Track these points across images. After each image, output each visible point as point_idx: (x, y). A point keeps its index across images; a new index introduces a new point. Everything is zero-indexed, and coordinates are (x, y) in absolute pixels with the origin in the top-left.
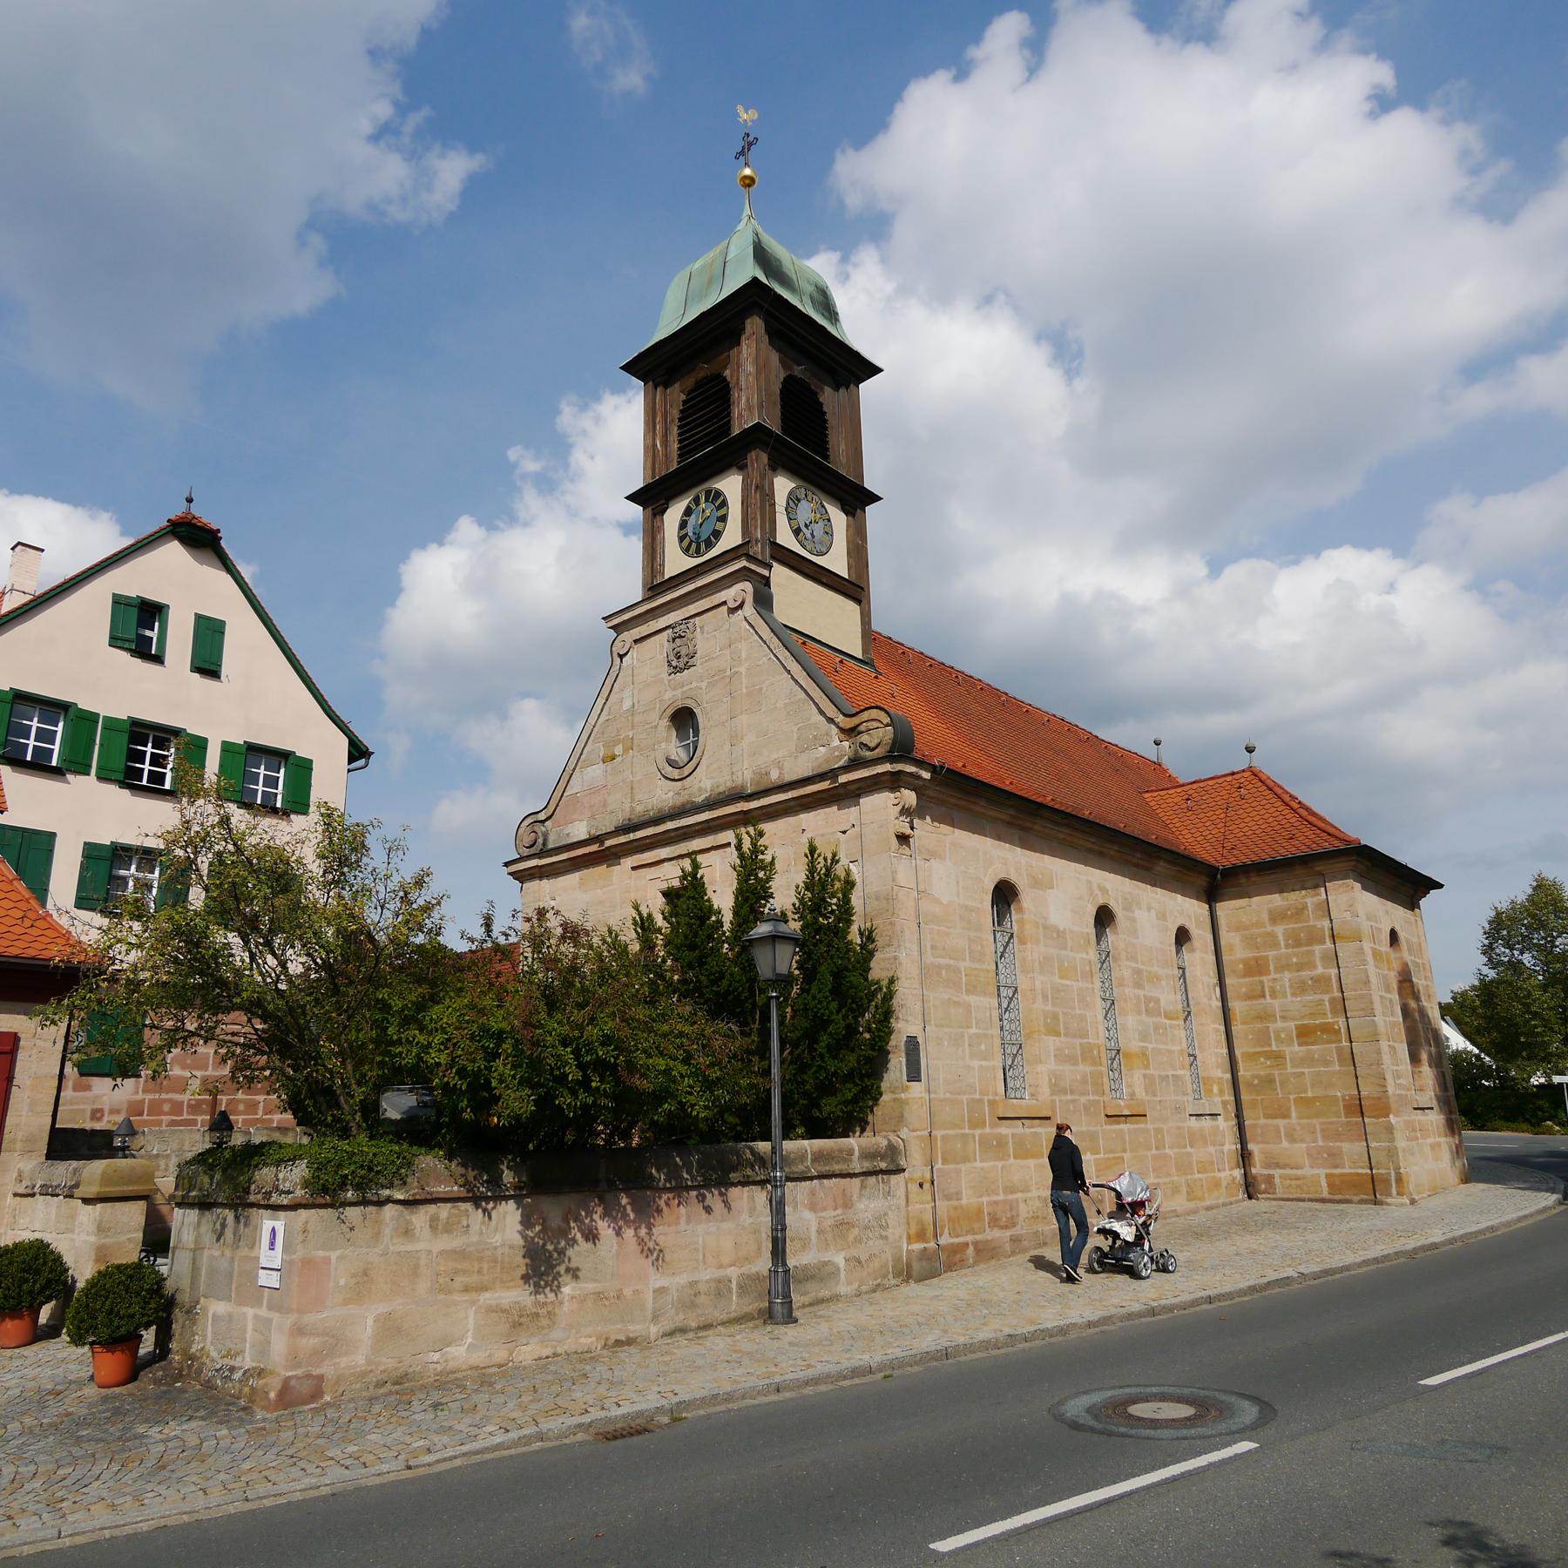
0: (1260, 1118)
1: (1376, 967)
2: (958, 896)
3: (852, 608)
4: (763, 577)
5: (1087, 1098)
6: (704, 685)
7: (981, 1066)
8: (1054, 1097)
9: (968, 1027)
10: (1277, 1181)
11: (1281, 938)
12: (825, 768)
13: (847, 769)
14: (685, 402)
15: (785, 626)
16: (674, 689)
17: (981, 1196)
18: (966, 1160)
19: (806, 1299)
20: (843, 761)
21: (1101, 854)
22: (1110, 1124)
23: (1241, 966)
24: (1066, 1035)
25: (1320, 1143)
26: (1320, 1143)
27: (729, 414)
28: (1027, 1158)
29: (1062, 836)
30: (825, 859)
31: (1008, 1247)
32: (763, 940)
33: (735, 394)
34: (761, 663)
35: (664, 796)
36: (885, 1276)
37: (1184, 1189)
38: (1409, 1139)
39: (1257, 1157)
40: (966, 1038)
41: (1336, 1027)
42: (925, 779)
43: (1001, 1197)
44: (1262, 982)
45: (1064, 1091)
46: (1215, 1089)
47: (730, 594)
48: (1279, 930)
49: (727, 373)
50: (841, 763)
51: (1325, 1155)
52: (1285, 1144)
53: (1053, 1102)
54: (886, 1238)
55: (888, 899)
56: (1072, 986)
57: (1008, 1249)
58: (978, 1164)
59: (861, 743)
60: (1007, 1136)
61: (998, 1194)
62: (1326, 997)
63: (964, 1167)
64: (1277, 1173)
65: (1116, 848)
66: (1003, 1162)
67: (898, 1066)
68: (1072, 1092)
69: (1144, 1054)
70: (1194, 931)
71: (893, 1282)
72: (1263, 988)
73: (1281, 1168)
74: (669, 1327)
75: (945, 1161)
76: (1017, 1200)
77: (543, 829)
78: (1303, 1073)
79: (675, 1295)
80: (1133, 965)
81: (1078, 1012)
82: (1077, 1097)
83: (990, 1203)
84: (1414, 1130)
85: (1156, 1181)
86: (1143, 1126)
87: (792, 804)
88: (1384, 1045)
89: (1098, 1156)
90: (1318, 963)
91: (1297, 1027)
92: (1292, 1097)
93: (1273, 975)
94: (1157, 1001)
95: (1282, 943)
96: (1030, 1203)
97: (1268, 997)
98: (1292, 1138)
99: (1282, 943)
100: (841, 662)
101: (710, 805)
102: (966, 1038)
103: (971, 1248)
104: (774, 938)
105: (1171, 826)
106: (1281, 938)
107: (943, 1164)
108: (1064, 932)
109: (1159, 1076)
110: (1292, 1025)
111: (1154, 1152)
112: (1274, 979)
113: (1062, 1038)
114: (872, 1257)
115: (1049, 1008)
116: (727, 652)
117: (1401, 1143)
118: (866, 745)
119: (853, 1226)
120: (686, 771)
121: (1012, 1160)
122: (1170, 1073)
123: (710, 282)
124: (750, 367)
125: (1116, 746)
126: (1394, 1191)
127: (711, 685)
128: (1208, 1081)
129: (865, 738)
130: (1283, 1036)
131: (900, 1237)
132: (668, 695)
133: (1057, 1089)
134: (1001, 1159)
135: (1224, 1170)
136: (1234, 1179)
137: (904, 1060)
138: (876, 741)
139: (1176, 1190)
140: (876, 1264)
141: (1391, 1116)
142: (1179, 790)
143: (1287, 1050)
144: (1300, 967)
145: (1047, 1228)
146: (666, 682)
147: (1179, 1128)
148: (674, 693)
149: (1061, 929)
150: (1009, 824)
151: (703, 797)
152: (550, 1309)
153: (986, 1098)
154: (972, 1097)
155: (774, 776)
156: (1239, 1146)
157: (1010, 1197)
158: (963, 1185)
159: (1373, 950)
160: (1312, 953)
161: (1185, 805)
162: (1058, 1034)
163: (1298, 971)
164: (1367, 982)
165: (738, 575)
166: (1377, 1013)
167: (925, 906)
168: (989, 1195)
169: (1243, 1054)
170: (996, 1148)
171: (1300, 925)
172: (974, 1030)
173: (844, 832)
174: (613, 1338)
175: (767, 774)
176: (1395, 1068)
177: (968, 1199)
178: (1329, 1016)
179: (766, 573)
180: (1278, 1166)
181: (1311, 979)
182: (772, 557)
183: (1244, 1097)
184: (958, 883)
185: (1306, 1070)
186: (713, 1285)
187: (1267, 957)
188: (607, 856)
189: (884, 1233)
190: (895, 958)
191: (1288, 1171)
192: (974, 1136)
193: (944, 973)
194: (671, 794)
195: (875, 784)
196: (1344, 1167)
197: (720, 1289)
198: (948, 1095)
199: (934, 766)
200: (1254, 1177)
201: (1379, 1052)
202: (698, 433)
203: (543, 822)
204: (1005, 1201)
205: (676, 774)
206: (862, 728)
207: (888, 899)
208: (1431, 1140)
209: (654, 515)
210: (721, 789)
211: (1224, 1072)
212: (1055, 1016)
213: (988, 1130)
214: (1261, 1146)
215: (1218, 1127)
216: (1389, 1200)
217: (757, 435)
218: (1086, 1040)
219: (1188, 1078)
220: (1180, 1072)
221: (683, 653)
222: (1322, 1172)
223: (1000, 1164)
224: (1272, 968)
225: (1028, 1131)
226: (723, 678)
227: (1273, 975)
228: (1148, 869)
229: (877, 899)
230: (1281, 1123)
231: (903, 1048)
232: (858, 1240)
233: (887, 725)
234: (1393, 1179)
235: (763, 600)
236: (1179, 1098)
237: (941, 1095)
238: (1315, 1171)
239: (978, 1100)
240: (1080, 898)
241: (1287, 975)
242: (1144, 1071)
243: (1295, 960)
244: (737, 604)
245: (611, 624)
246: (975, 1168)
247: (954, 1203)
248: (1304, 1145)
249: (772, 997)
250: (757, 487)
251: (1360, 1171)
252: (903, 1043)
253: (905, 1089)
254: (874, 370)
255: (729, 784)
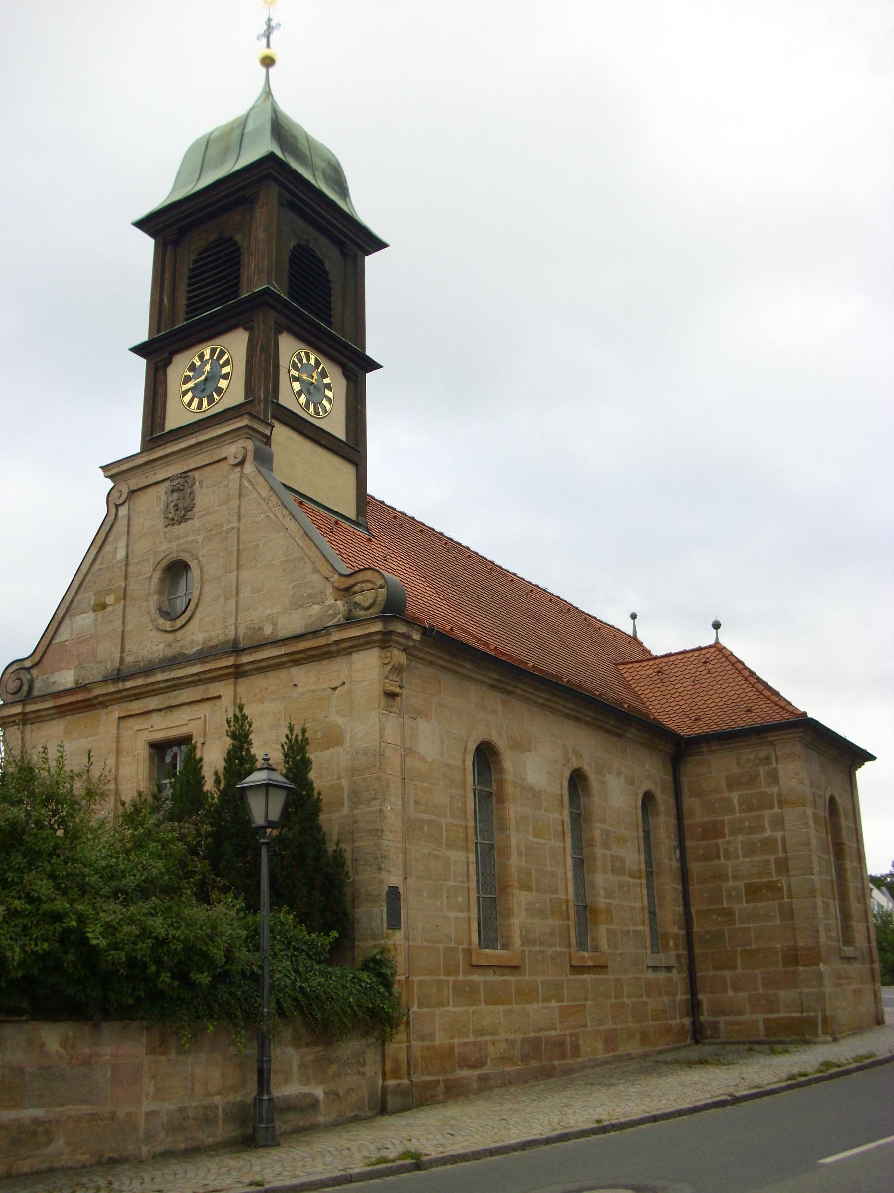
0: (709, 970)
1: (816, 830)
2: (442, 754)
3: (347, 471)
4: (265, 436)
5: (555, 949)
6: (200, 538)
7: (458, 917)
8: (523, 948)
9: (446, 880)
10: (722, 1026)
11: (736, 803)
12: (318, 626)
13: (340, 627)
14: (195, 262)
15: (282, 484)
16: (170, 542)
17: (452, 1038)
18: (441, 1004)
19: (286, 1127)
20: (336, 620)
21: (577, 720)
22: (574, 974)
23: (700, 829)
24: (538, 890)
25: (761, 991)
26: (761, 991)
27: (238, 277)
28: (496, 1004)
29: (541, 701)
30: (286, 743)
31: (475, 1085)
32: (256, 787)
33: (245, 258)
34: (258, 520)
35: (155, 648)
36: (361, 1108)
37: (638, 1036)
38: (836, 985)
39: (705, 1006)
40: (445, 890)
41: (779, 885)
42: (416, 641)
43: (472, 1039)
44: (717, 844)
45: (532, 943)
46: (671, 944)
47: (232, 450)
48: (735, 796)
49: (238, 237)
50: (335, 622)
51: (764, 1002)
52: (730, 993)
53: (523, 952)
54: (363, 1074)
55: (375, 755)
56: (545, 844)
57: (475, 1086)
58: (451, 1008)
59: (355, 603)
60: (479, 983)
61: (469, 1037)
62: (772, 858)
63: (437, 1011)
64: (722, 1019)
65: (591, 714)
66: (475, 1007)
67: (379, 915)
68: (541, 944)
69: (608, 910)
70: (659, 796)
71: (368, 1114)
72: (718, 849)
73: (725, 1015)
74: (159, 1149)
75: (420, 1005)
76: (486, 1042)
77: (29, 676)
78: (749, 928)
79: (165, 1118)
80: (603, 826)
81: (549, 869)
82: (546, 949)
83: (461, 1045)
84: (840, 978)
85: (614, 1027)
86: (603, 976)
87: (285, 659)
88: (819, 901)
89: (563, 1004)
90: (767, 826)
91: (746, 886)
92: (739, 950)
93: (727, 838)
94: (623, 860)
95: (737, 808)
96: (498, 1045)
97: (722, 859)
98: (736, 988)
99: (737, 808)
100: (336, 523)
101: (204, 655)
102: (445, 890)
103: (442, 1085)
104: (268, 786)
105: (642, 697)
106: (736, 803)
107: (418, 1007)
108: (540, 793)
109: (622, 930)
110: (741, 884)
111: (613, 1000)
112: (728, 842)
113: (534, 893)
114: (349, 1090)
115: (524, 864)
116: (225, 507)
117: (828, 989)
118: (359, 605)
119: (333, 1063)
120: (179, 623)
121: (482, 1006)
122: (632, 928)
123: (226, 151)
124: (261, 235)
125: (595, 618)
126: (820, 1031)
127: (207, 539)
128: (664, 935)
129: (358, 598)
130: (733, 894)
131: (376, 1073)
132: (164, 547)
133: (527, 941)
134: (473, 1004)
135: (675, 1018)
136: (684, 1026)
137: (385, 909)
138: (370, 601)
139: (631, 1036)
140: (353, 1098)
141: (821, 965)
142: (651, 663)
143: (736, 907)
144: (751, 830)
145: (513, 1068)
146: (162, 534)
147: (637, 979)
148: (170, 545)
149: (537, 790)
150: (493, 687)
151: (194, 650)
152: (48, 1127)
153: (461, 947)
154: (447, 945)
155: (268, 631)
156: (689, 996)
157: (480, 1039)
158: (437, 1027)
159: (814, 814)
160: (761, 817)
161: (657, 677)
162: (530, 889)
163: (749, 834)
164: (807, 844)
165: (241, 432)
166: (814, 872)
167: (410, 762)
168: (460, 1037)
169: (698, 911)
170: (468, 993)
171: (753, 791)
172: (451, 883)
173: (334, 689)
174: (107, 1155)
175: (261, 629)
176: (826, 921)
177: (440, 1039)
178: (774, 875)
179: (268, 433)
180: (724, 1013)
181: (760, 841)
182: (274, 417)
183: (698, 951)
184: (442, 742)
185: (752, 925)
186: (201, 1111)
187: (723, 820)
188: (94, 705)
189: (361, 1070)
190: (381, 811)
191: (732, 1018)
192: (448, 982)
193: (426, 827)
194: (162, 646)
195: (367, 643)
196: (779, 1012)
197: (207, 1118)
198: (425, 944)
199: (424, 628)
200: (701, 1024)
201: (814, 906)
202: (208, 291)
203: (28, 669)
204: (475, 1043)
205: (168, 625)
206: (356, 588)
207: (375, 755)
208: (853, 987)
209: (157, 369)
210: (214, 642)
211: (680, 928)
212: (528, 874)
213: (461, 977)
214: (710, 995)
215: (672, 978)
216: (817, 1040)
217: (265, 299)
218: (555, 896)
219: (648, 933)
220: (641, 928)
221: (180, 506)
222: (760, 1017)
223: (471, 1009)
224: (727, 831)
225: (499, 978)
226: (220, 533)
227: (727, 838)
228: (619, 735)
229: (365, 754)
230: (728, 973)
231: (385, 897)
232: (337, 1075)
233: (381, 587)
234: (820, 1020)
235: (264, 459)
236: (639, 951)
237: (419, 944)
238: (755, 1016)
239: (452, 948)
240: (556, 761)
241: (740, 838)
242: (608, 926)
243: (747, 824)
244: (238, 461)
245: (110, 473)
246: (449, 1012)
247: (427, 1043)
248: (746, 994)
249: (263, 843)
250: (262, 349)
251: (793, 1014)
252: (385, 893)
253: (387, 937)
254: (378, 244)
255: (221, 638)
